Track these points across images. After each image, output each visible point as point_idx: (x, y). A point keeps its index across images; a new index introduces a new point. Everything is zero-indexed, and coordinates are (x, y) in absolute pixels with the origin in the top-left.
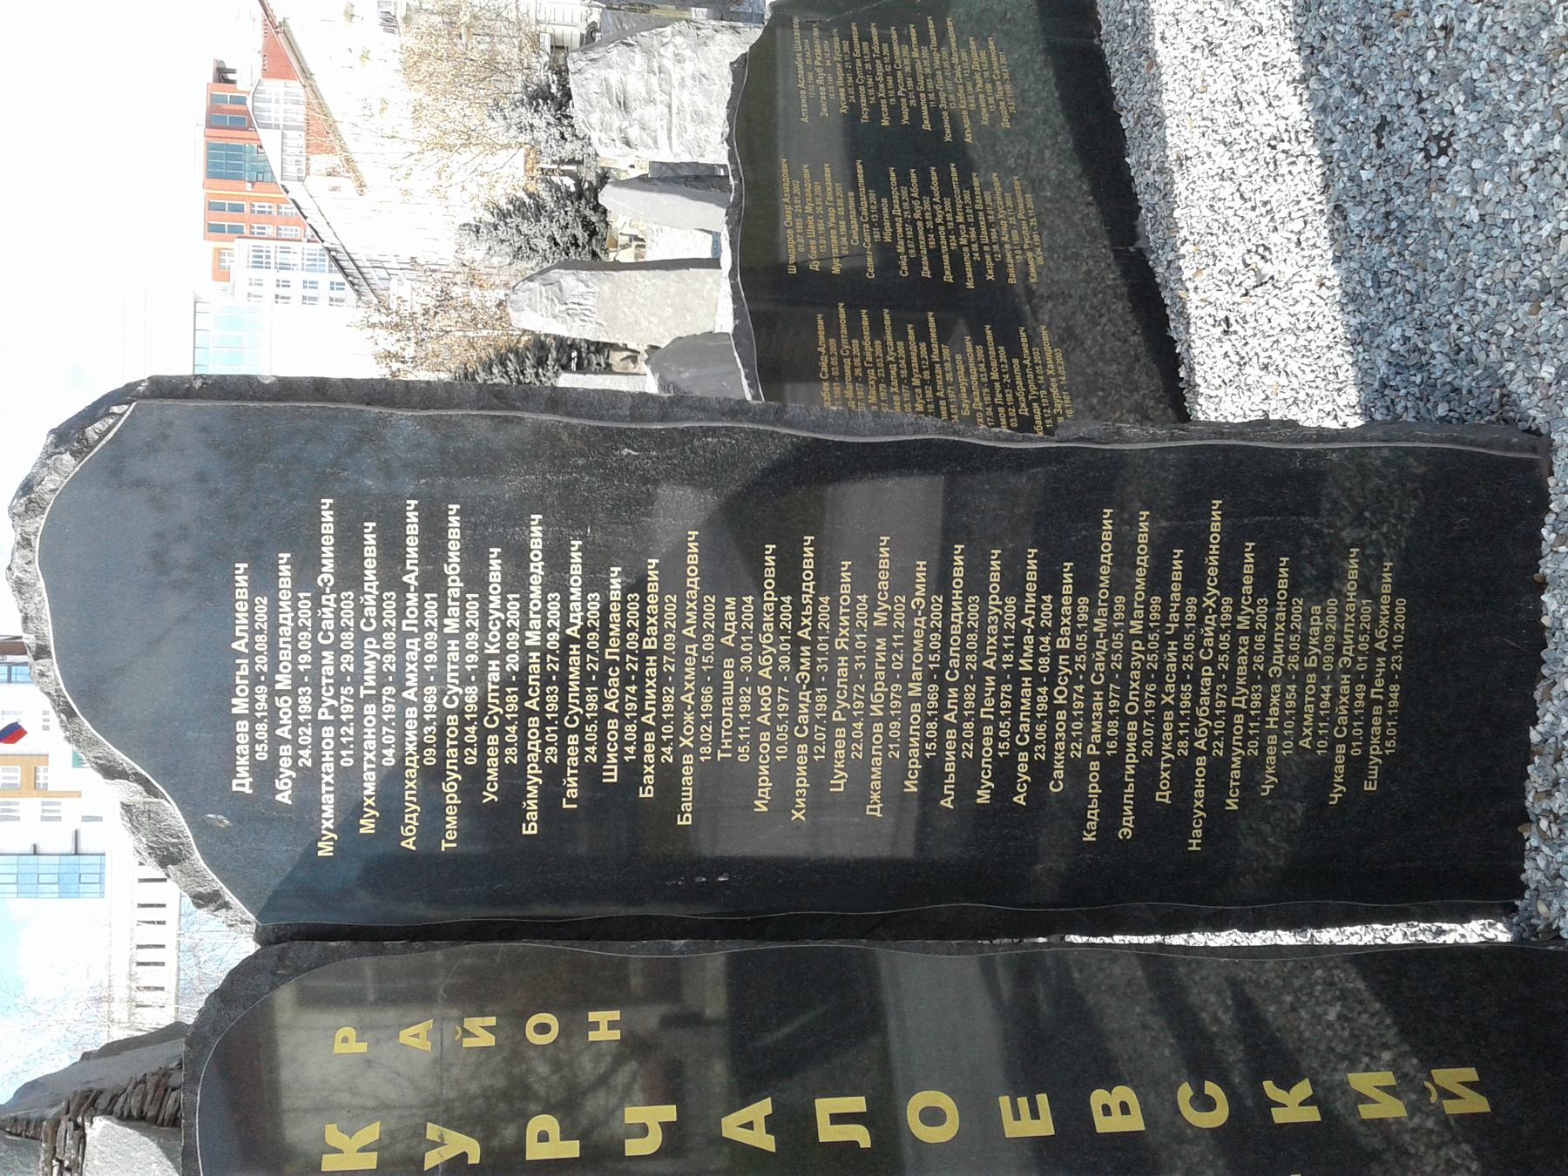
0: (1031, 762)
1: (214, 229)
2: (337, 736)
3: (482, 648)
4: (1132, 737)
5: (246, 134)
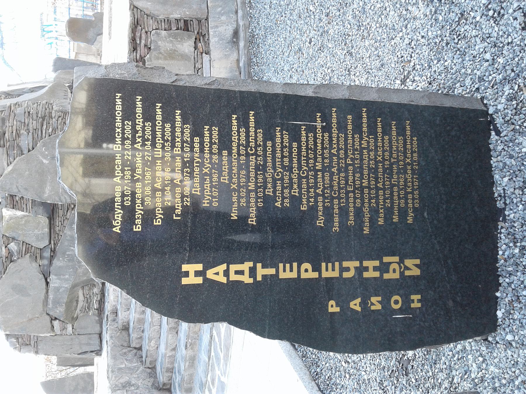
3: (376, 158)
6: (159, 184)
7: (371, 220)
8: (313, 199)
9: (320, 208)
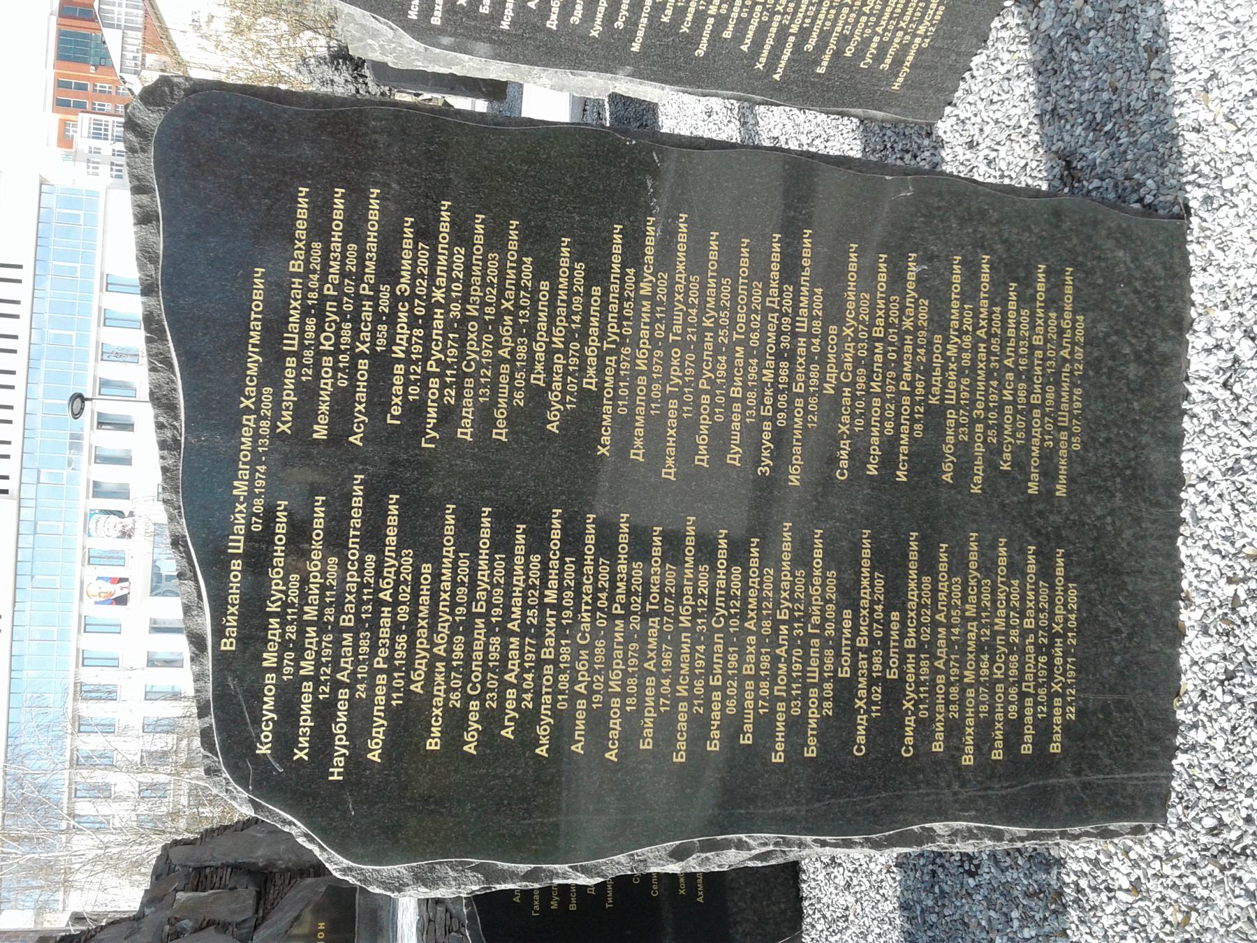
0: (589, 710)
1: (60, 104)
4: (650, 692)
5: (92, 25)
6: (614, 753)
9: (673, 422)
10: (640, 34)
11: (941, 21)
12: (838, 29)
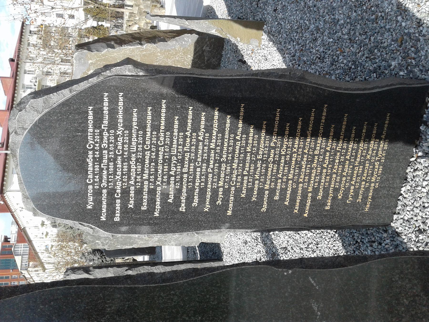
2: (188, 178)
4: (245, 182)
5: (12, 256)
7: (187, 199)
8: (127, 153)
10: (231, 205)
11: (382, 173)
12: (332, 186)
